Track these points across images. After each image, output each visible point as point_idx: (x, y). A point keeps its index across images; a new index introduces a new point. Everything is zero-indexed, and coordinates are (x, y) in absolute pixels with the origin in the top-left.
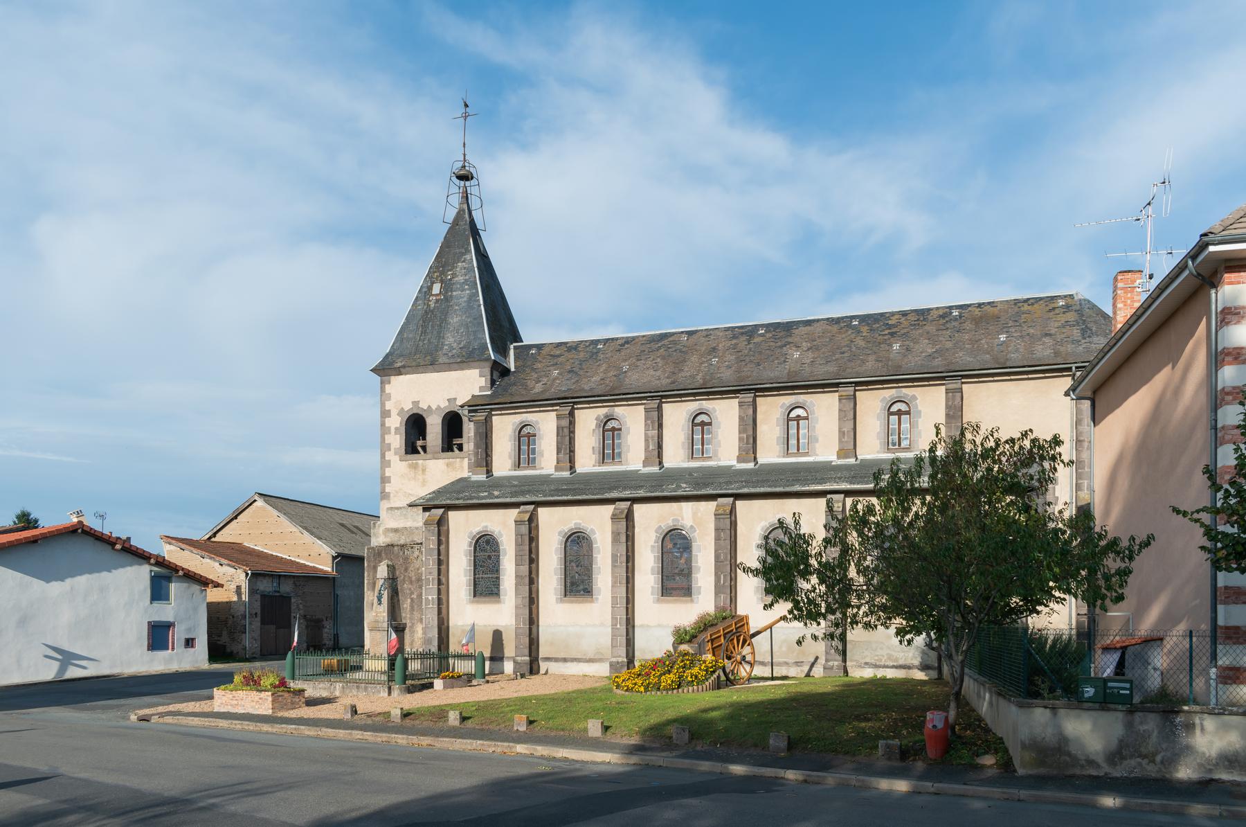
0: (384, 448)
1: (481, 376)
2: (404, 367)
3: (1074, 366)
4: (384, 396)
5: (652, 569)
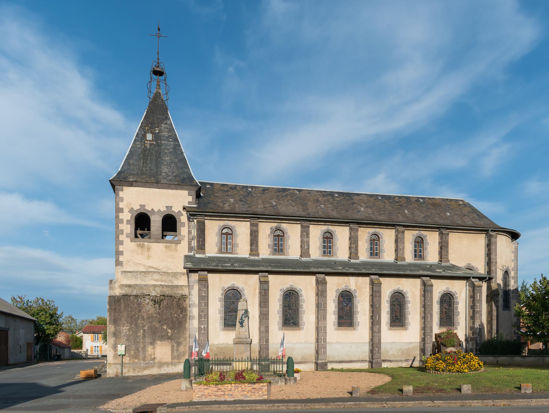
0: (119, 232)
1: (122, 190)
2: (136, 181)
3: (490, 229)
4: (118, 200)
5: (334, 312)
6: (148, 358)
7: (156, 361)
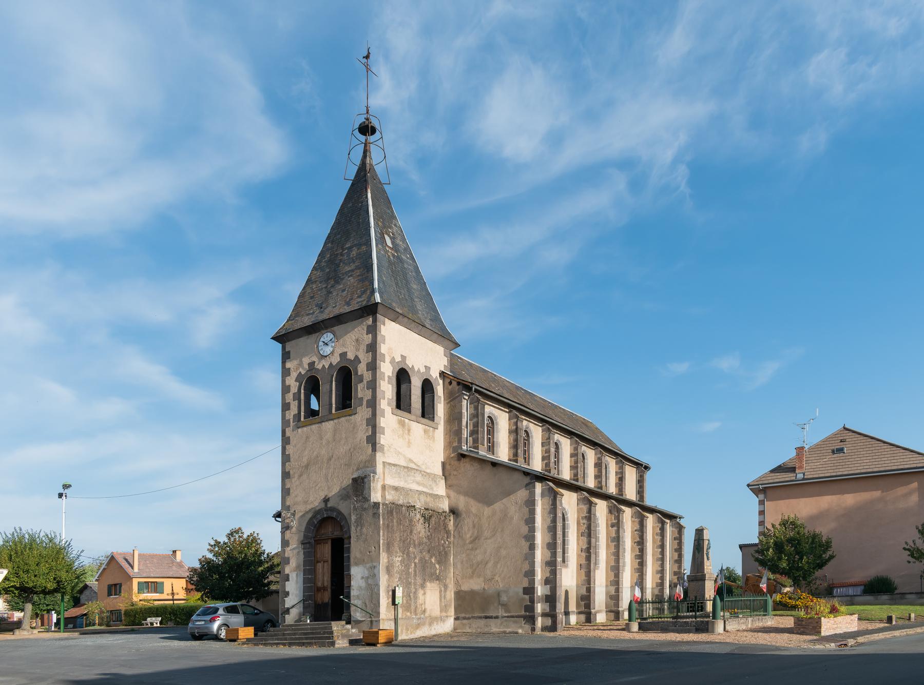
6: (419, 611)
7: (427, 614)
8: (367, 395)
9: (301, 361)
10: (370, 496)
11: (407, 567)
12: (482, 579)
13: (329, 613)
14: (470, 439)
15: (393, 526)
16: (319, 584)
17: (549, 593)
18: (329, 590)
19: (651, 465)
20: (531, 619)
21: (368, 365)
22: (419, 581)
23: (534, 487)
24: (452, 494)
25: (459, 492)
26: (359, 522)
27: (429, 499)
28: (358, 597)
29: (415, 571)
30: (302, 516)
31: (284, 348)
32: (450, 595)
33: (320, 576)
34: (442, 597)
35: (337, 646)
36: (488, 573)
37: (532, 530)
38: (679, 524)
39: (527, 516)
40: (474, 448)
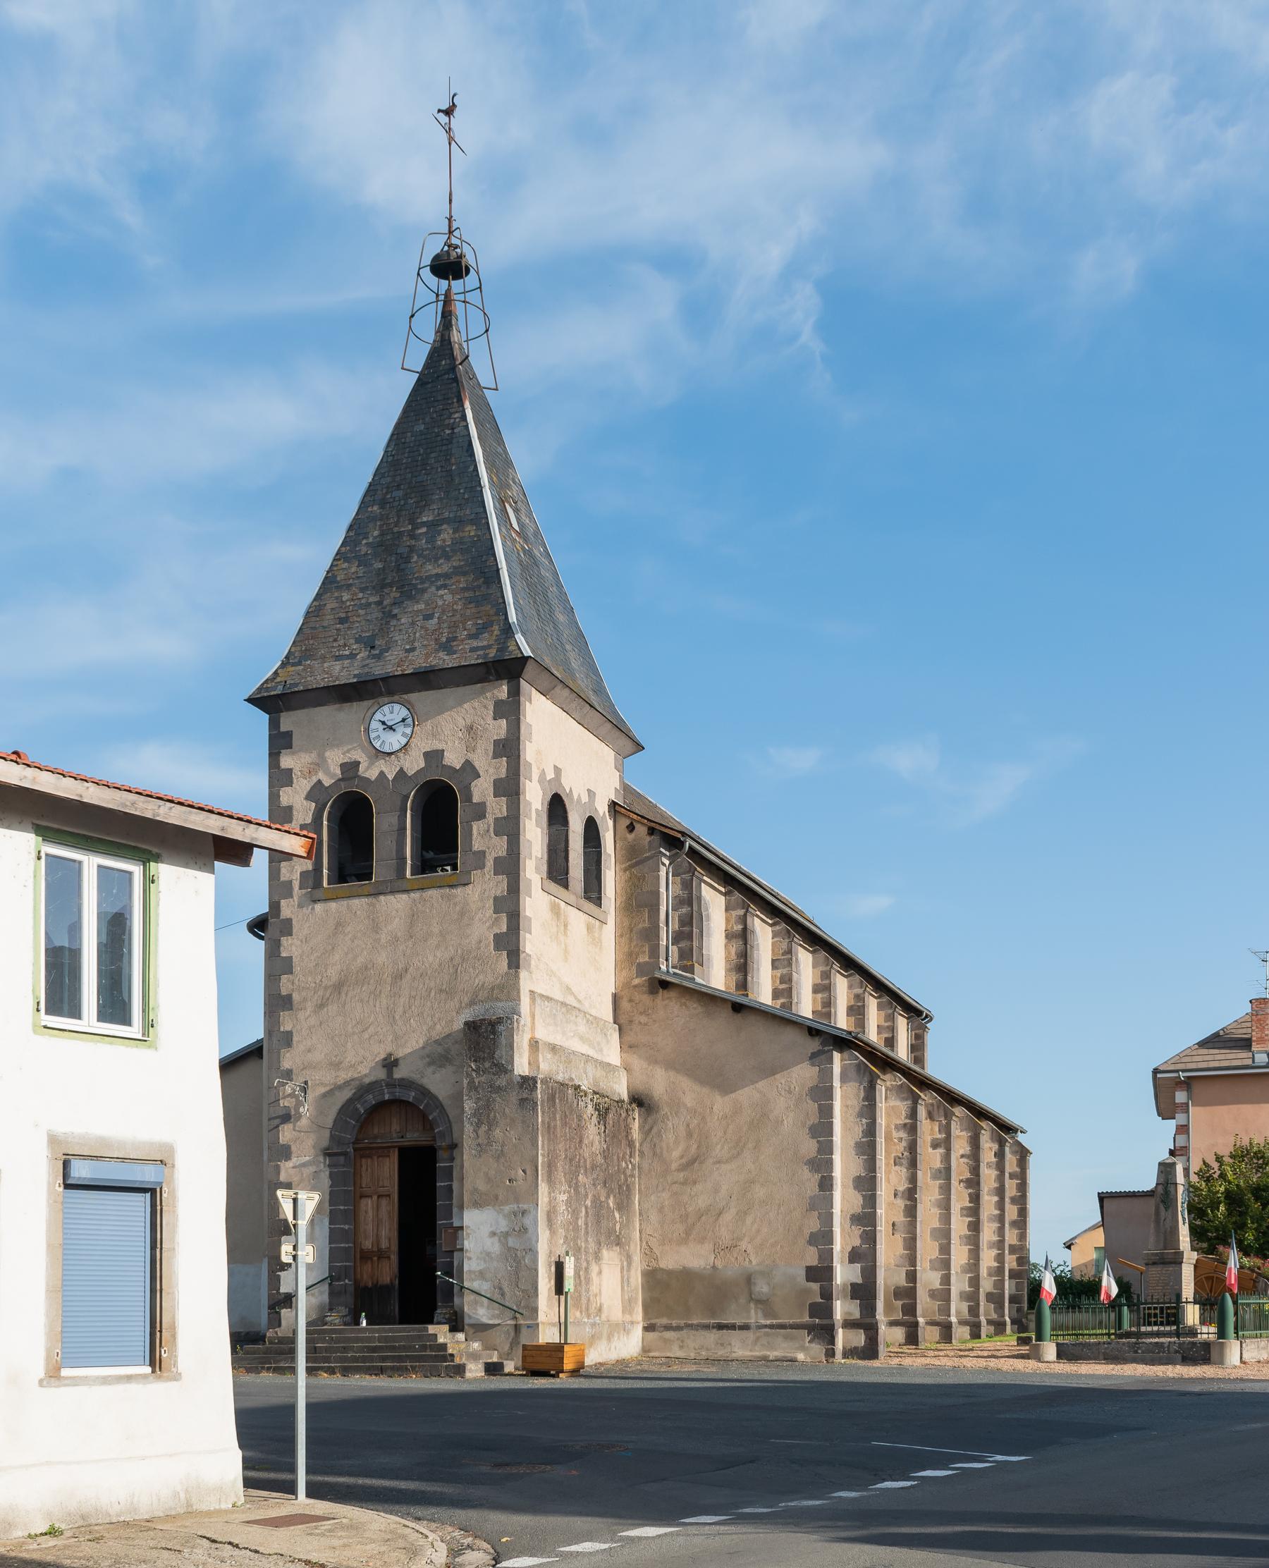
6: (592, 1310)
7: (604, 1317)
8: (499, 847)
9: (321, 756)
10: (511, 1061)
11: (575, 1213)
12: (708, 1246)
13: (395, 1308)
14: (674, 950)
15: (555, 1126)
16: (368, 1244)
17: (860, 1281)
18: (394, 1258)
19: (934, 1013)
20: (825, 1333)
21: (497, 783)
22: (592, 1246)
23: (831, 1061)
24: (637, 1062)
25: (653, 1061)
26: (484, 1116)
27: (600, 1073)
28: (481, 1275)
29: (586, 1224)
30: (324, 1095)
31: (274, 724)
32: (637, 1278)
33: (368, 1226)
34: (625, 1281)
35: (468, 1375)
36: (725, 1235)
37: (826, 1148)
38: (1020, 1144)
39: (814, 1119)
40: (684, 968)
